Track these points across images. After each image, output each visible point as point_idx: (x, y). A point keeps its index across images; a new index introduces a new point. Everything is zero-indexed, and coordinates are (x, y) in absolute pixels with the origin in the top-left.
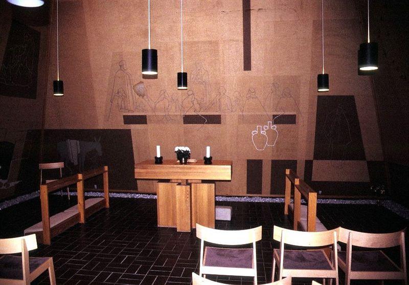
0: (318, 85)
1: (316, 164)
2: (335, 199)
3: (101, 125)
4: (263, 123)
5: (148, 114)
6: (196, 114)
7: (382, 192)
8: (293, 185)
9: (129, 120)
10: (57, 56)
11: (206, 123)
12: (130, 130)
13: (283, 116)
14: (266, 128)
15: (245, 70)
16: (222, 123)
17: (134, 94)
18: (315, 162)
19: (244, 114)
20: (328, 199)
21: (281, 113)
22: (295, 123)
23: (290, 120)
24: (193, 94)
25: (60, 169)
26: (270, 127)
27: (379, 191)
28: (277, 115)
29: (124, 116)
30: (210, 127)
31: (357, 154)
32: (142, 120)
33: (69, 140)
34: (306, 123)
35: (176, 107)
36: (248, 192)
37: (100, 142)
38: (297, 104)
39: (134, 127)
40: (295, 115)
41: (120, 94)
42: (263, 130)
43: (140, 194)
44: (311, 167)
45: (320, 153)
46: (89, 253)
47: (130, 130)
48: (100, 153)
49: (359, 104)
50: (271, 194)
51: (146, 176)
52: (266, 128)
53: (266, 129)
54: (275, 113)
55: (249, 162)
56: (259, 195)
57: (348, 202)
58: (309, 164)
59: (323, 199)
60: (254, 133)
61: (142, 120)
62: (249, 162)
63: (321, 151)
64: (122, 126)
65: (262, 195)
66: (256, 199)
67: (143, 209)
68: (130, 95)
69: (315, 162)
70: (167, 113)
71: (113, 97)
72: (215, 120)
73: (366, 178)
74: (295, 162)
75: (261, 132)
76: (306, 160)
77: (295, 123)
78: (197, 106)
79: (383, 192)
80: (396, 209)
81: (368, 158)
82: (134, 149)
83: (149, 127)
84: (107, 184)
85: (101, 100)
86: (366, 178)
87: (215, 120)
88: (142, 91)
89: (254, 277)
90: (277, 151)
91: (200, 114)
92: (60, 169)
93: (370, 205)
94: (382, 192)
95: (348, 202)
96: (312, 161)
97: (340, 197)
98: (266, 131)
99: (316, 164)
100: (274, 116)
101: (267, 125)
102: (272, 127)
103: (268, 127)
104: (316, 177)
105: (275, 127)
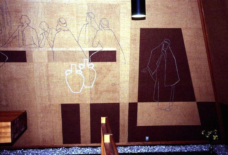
1: (143, 107)
2: (163, 145)
7: (215, 137)
11: (8, 61)
13: (101, 52)
14: (82, 67)
16: (28, 60)
19: (54, 49)
20: (156, 145)
21: (98, 49)
22: (115, 61)
27: (211, 136)
28: (97, 51)
31: (184, 93)
34: (128, 60)
36: (64, 143)
38: (117, 39)
42: (78, 69)
45: (145, 95)
49: (187, 37)
50: (92, 142)
52: (82, 67)
56: (77, 145)
57: (177, 149)
58: (133, 108)
59: (151, 146)
63: (147, 90)
65: (80, 145)
66: (73, 151)
67: (159, 16)
73: (196, 121)
74: (116, 106)
76: (129, 103)
77: (115, 61)
79: (216, 138)
81: (199, 97)
86: (196, 121)
89: (142, 30)
90: (96, 93)
93: (203, 152)
94: (215, 137)
95: (177, 149)
97: (170, 142)
99: (143, 107)
101: (82, 62)
104: (142, 121)
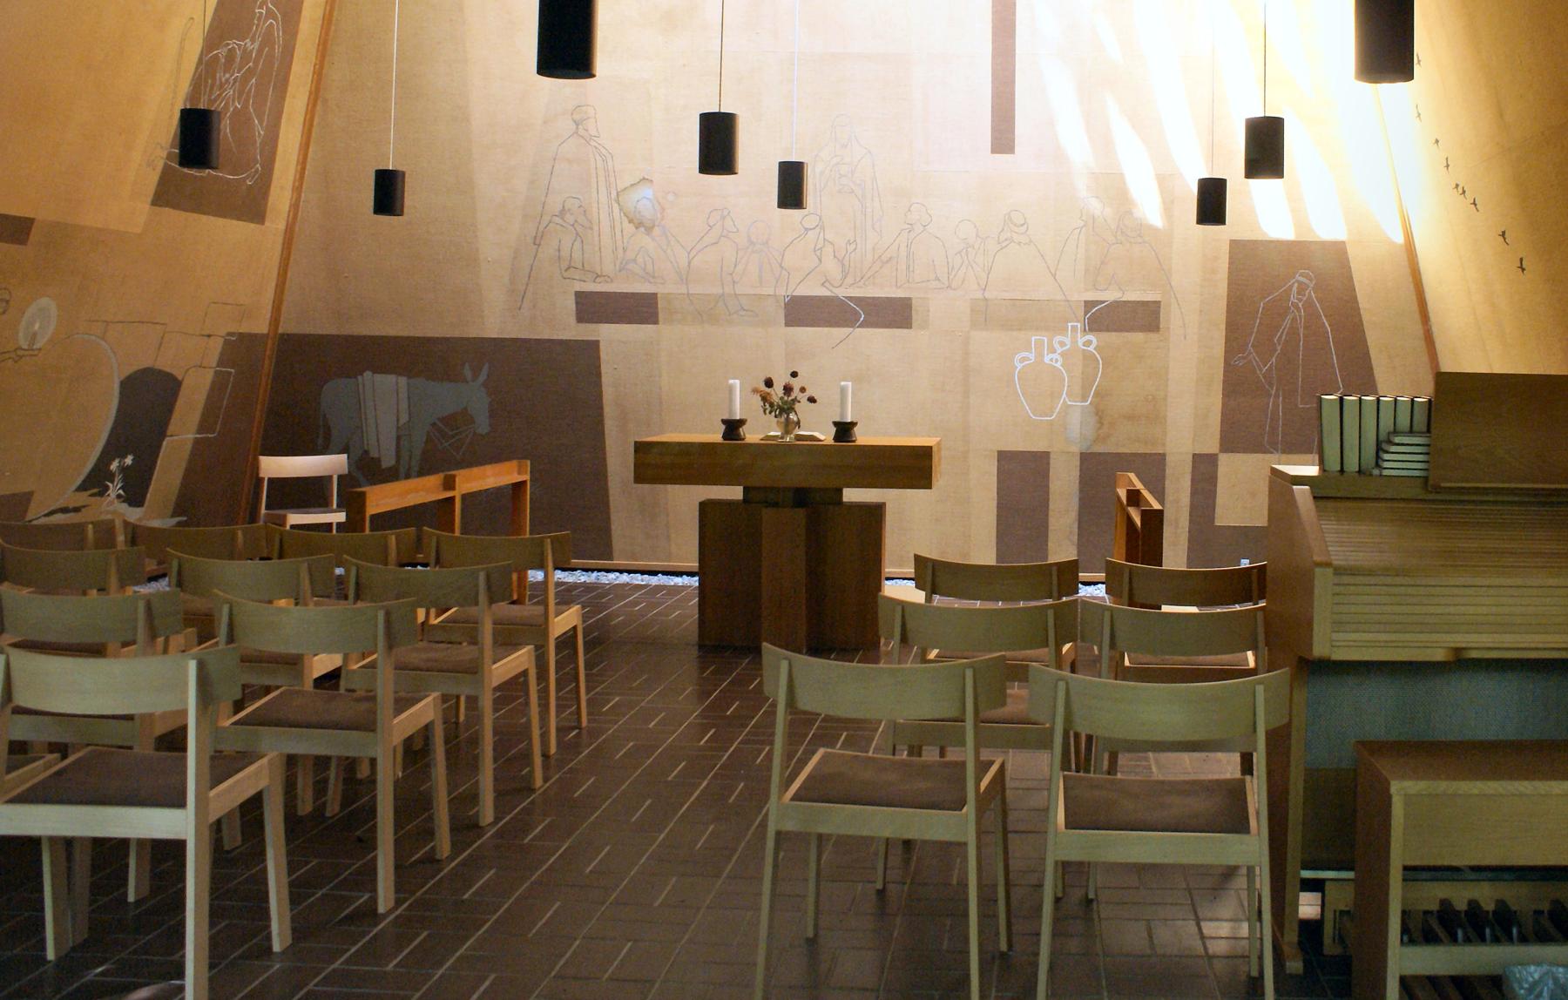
0: (30, 229)
3: (495, 320)
4: (1054, 325)
6: (828, 293)
8: (256, 62)
9: (594, 307)
11: (864, 325)
12: (594, 346)
13: (1117, 305)
14: (1062, 344)
15: (994, 151)
17: (617, 224)
18: (1224, 459)
19: (987, 295)
21: (1110, 296)
23: (1143, 317)
25: (331, 477)
26: (1074, 342)
30: (875, 341)
33: (368, 374)
37: (485, 385)
39: (611, 336)
40: (1158, 303)
41: (570, 218)
43: (621, 572)
44: (1213, 479)
46: (390, 967)
47: (594, 346)
48: (483, 425)
51: (669, 557)
52: (1062, 344)
53: (1062, 350)
54: (1091, 296)
60: (1022, 360)
61: (640, 309)
62: (1004, 457)
64: (569, 329)
69: (1224, 459)
72: (893, 313)
75: (1047, 359)
85: (495, 243)
87: (893, 313)
88: (646, 209)
91: (842, 293)
92: (331, 477)
98: (1062, 354)
100: (1089, 304)
103: (1068, 341)
105: (1092, 342)
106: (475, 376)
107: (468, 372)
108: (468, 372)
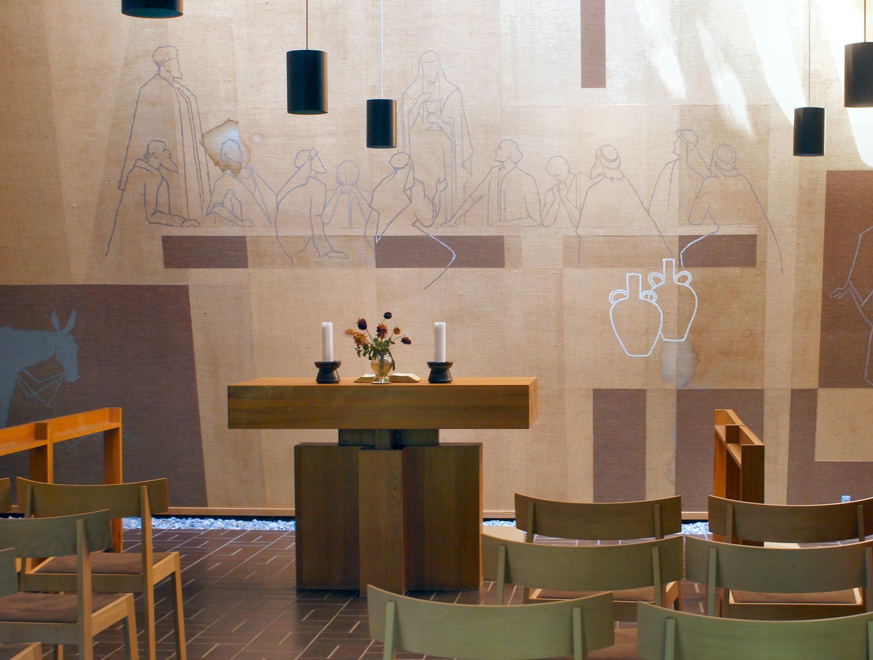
3: (81, 268)
5: (254, 231)
9: (182, 252)
10: (188, 565)
13: (711, 241)
14: (657, 280)
19: (581, 232)
21: (705, 230)
23: (741, 251)
24: (410, 165)
26: (669, 278)
28: (699, 237)
29: (166, 240)
32: (229, 252)
35: (350, 209)
37: (72, 332)
39: (199, 280)
40: (753, 238)
41: (155, 162)
42: (647, 287)
52: (657, 280)
55: (601, 396)
58: (803, 404)
60: (618, 297)
61: (229, 252)
62: (601, 396)
64: (158, 275)
68: (189, 158)
70: (318, 232)
71: (126, 171)
72: (486, 252)
75: (641, 296)
78: (421, 206)
80: (697, 530)
82: (198, 355)
83: (254, 278)
84: (825, 593)
87: (486, 252)
88: (232, 152)
96: (820, 386)
98: (657, 291)
99: (832, 403)
100: (683, 240)
101: (658, 266)
102: (675, 278)
106: (63, 325)
107: (55, 321)
108: (55, 321)
